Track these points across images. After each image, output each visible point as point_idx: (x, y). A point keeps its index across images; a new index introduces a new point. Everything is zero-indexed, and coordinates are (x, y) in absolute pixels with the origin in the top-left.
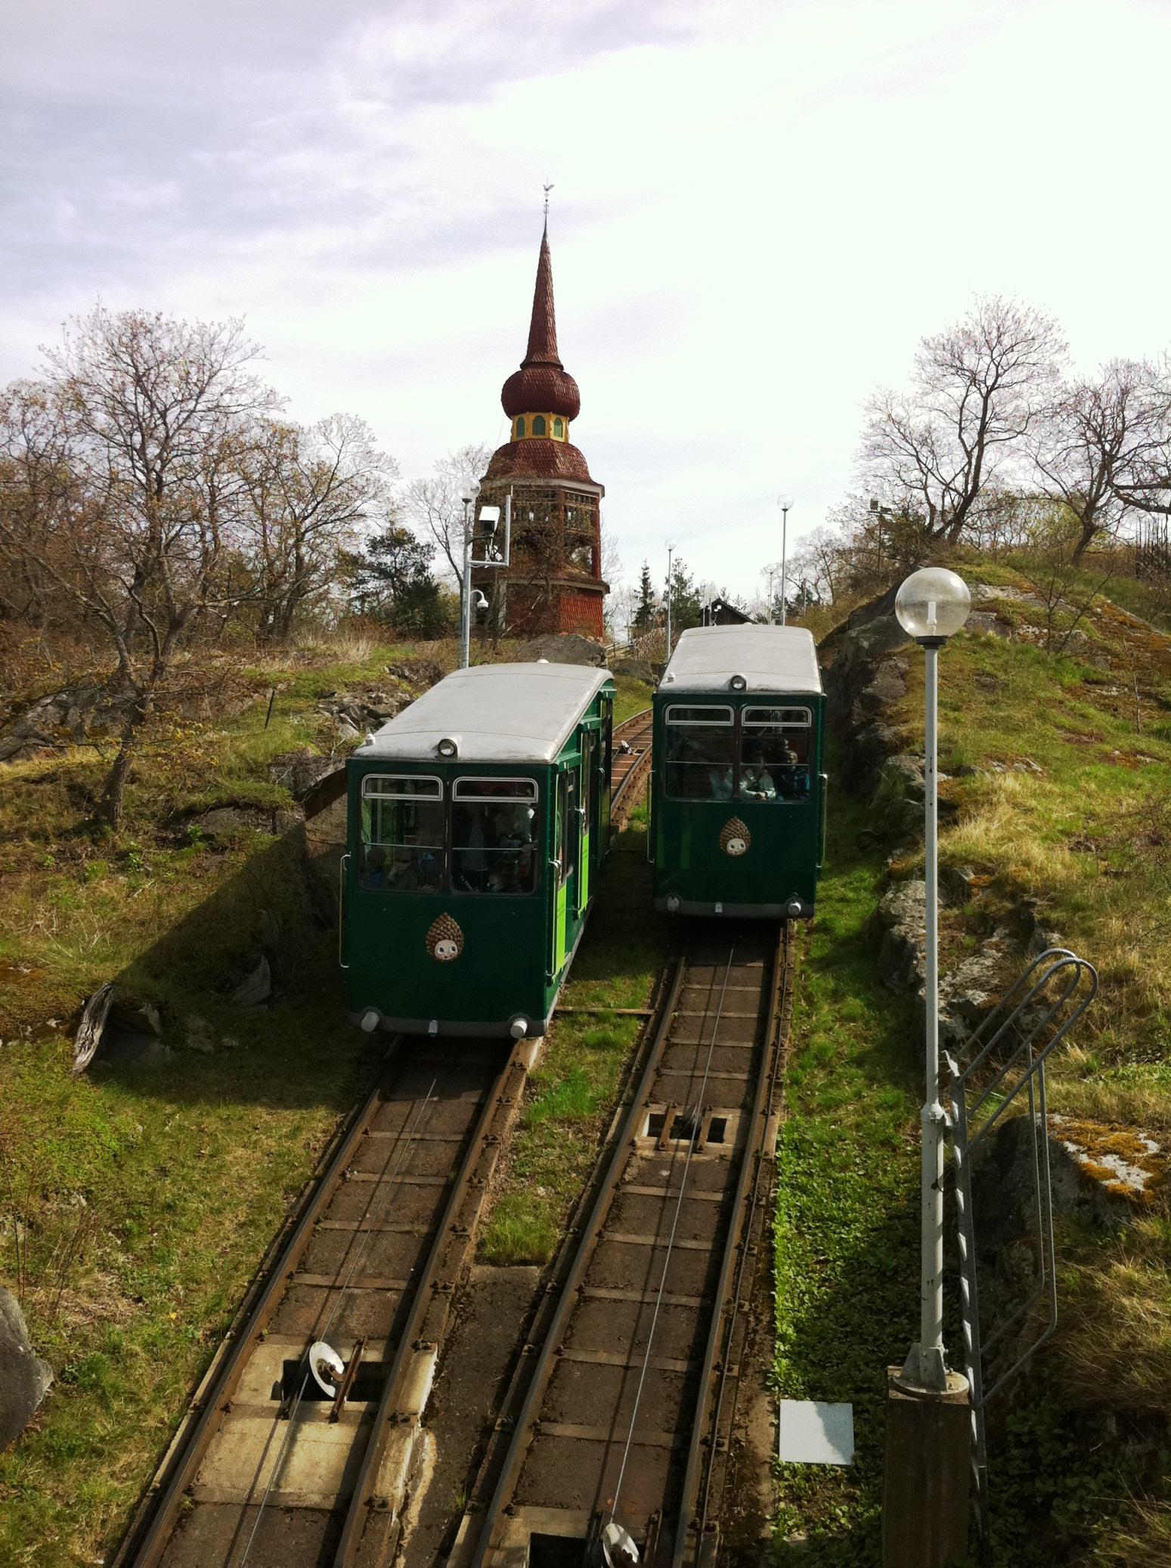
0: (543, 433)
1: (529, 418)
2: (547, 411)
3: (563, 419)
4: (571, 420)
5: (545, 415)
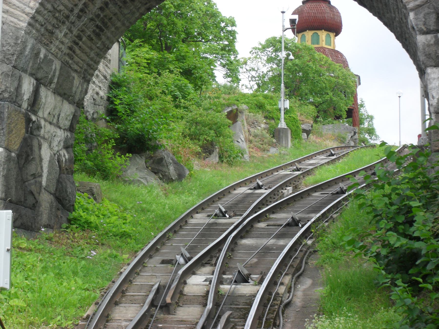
0: (318, 43)
1: (309, 34)
2: (320, 29)
3: (332, 35)
4: (336, 35)
5: (319, 32)
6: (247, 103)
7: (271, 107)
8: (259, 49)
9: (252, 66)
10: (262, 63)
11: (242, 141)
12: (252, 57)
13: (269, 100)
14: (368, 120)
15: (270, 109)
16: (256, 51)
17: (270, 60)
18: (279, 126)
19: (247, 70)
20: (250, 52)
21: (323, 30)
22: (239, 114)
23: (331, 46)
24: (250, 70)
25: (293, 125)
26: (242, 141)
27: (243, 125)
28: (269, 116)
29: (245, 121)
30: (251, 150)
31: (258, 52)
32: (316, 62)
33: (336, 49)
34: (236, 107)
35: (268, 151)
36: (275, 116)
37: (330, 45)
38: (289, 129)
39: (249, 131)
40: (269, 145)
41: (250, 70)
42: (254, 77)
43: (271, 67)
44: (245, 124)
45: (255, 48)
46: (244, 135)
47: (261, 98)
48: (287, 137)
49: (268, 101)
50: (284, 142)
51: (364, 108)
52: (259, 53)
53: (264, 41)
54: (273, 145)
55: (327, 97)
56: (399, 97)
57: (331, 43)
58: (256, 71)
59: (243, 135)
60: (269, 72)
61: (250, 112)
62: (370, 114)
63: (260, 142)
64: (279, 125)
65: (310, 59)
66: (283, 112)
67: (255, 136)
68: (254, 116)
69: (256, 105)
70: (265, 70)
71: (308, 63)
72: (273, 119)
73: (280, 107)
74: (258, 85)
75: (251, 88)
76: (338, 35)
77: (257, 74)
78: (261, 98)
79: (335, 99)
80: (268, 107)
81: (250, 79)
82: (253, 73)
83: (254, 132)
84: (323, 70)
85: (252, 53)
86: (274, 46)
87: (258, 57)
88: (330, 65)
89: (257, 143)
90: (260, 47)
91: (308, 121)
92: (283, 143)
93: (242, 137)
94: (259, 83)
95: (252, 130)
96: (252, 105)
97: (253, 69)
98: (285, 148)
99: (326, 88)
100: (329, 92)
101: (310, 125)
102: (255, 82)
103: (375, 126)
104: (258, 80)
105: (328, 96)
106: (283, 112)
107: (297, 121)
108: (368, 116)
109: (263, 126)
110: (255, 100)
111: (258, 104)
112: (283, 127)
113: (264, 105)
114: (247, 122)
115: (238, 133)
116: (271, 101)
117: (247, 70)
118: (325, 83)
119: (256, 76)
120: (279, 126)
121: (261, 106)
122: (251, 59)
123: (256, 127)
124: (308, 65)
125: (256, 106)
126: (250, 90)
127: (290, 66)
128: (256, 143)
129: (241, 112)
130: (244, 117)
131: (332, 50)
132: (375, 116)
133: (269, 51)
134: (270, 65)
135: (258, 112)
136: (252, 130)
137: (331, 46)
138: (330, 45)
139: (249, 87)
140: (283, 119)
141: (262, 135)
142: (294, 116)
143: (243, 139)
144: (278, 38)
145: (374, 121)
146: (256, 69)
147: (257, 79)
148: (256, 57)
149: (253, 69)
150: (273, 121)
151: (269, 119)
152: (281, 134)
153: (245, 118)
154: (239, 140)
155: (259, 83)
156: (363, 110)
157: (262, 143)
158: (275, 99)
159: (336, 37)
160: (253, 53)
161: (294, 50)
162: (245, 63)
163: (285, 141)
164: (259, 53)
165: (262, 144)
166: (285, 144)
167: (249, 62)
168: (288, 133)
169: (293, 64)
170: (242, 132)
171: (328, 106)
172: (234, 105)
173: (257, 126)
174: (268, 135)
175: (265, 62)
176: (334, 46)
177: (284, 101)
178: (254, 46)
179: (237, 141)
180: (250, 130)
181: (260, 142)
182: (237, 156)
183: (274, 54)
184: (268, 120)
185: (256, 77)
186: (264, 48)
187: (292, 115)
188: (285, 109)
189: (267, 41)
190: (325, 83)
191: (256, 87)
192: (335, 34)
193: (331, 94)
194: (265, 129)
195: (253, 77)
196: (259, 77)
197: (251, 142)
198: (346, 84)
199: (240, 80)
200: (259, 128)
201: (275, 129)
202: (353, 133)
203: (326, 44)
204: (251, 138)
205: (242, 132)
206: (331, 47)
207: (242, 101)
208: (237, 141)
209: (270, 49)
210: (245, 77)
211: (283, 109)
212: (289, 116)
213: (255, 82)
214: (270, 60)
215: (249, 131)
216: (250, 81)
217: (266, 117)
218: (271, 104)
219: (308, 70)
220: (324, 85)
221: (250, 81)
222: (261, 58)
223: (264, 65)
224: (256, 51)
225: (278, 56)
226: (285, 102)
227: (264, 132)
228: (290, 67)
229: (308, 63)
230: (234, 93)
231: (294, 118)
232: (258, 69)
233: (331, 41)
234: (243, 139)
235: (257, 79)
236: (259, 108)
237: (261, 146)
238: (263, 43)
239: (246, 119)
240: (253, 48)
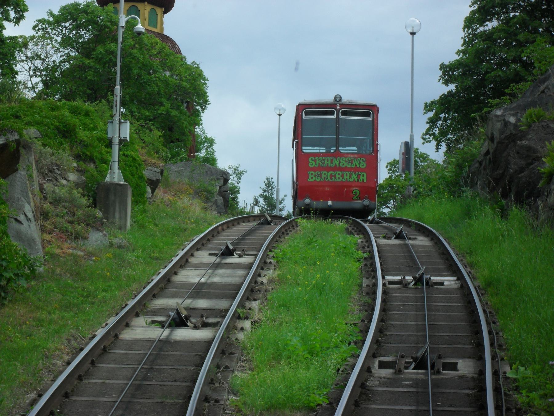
3: (159, 11)
4: (166, 12)
6: (38, 123)
7: (87, 133)
8: (49, 23)
9: (38, 49)
10: (53, 47)
11: (28, 220)
12: (37, 35)
13: (82, 117)
14: (205, 145)
15: (85, 139)
16: (44, 26)
17: (66, 42)
18: (108, 179)
19: (27, 57)
20: (34, 28)
21: (146, 3)
22: (22, 151)
23: (156, 28)
24: (33, 58)
25: (133, 175)
26: (28, 220)
27: (30, 177)
28: (84, 153)
29: (34, 167)
30: (48, 237)
31: (46, 28)
32: (143, 49)
33: (165, 33)
34: (17, 137)
35: (86, 238)
36: (96, 154)
37: (156, 26)
38: (129, 186)
39: (42, 189)
40: (88, 225)
41: (33, 58)
42: (39, 69)
43: (68, 55)
44: (35, 174)
45: (42, 21)
46: (32, 204)
47: (66, 113)
48: (124, 204)
49: (80, 120)
50: (117, 215)
51: (201, 127)
52: (49, 30)
53: (58, 9)
54: (98, 225)
55: (162, 110)
56: (280, 115)
57: (157, 23)
58: (43, 60)
59: (29, 204)
60: (64, 62)
61: (44, 145)
62: (209, 136)
63: (66, 218)
64: (108, 176)
65: (134, 46)
66: (116, 148)
67: (56, 202)
68: (53, 154)
69: (57, 128)
70: (57, 58)
71: (131, 50)
72: (91, 159)
73: (110, 136)
74: (45, 83)
75: (33, 88)
76: (168, 11)
77: (45, 65)
78: (66, 113)
79: (174, 113)
80: (83, 134)
81: (31, 73)
82: (38, 63)
83: (54, 192)
84: (156, 62)
85: (37, 29)
86: (75, 20)
87: (47, 36)
88: (167, 55)
89: (61, 220)
90: (51, 19)
91: (153, 161)
92: (114, 217)
93: (28, 209)
94: (46, 80)
95: (48, 186)
96: (49, 128)
97: (38, 57)
98: (120, 228)
99: (159, 93)
100: (164, 100)
101: (159, 170)
102: (40, 79)
103: (217, 155)
104: (45, 75)
105: (162, 108)
106: (116, 148)
107: (140, 165)
108: (206, 138)
109: (72, 177)
110: (55, 117)
111: (61, 128)
112: (116, 181)
113: (74, 130)
114: (37, 166)
115: (19, 199)
116: (87, 121)
117: (27, 57)
118: (158, 86)
119: (42, 68)
120: (108, 179)
121: (68, 131)
122: (35, 40)
123: (56, 179)
124: (131, 54)
125: (56, 132)
126: (31, 92)
127: (101, 53)
128: (58, 219)
129: (27, 147)
130: (33, 159)
131: (159, 34)
132: (217, 140)
133: (66, 28)
134: (66, 51)
135: (62, 144)
136: (48, 186)
137: (156, 28)
138: (156, 26)
139: (30, 85)
140: (117, 164)
141: (72, 201)
142: (134, 155)
143: (30, 215)
144: (82, 6)
145: (215, 147)
146: (43, 56)
147: (43, 73)
148: (43, 37)
149: (38, 57)
150: (92, 165)
151: (85, 161)
152: (112, 197)
153: (34, 161)
154: (22, 218)
155: (46, 80)
156: (198, 130)
157: (71, 219)
158: (94, 116)
159: (165, 15)
160: (39, 30)
161: (108, 28)
162: (25, 45)
163: (120, 212)
164: (49, 30)
165: (72, 223)
166: (120, 218)
167: (30, 45)
168: (126, 196)
169: (106, 51)
170: (27, 197)
171: (163, 125)
172: (12, 131)
173: (58, 177)
174: (84, 201)
175: (57, 46)
176: (162, 29)
177: (120, 123)
178: (39, 18)
179: (16, 220)
180: (45, 186)
181: (66, 218)
182: (17, 275)
183: (74, 32)
184: (82, 163)
185: (42, 71)
186: (58, 21)
187: (129, 152)
188: (122, 141)
189: (64, 9)
190: (158, 86)
191: (41, 86)
192: (163, 9)
193: (168, 105)
194: (77, 185)
195: (36, 69)
196: (46, 69)
197: (45, 215)
198: (195, 89)
199: (462, 38)
200: (64, 182)
201: (98, 184)
202: (222, 181)
203: (149, 25)
204: (46, 206)
205: (27, 197)
206: (157, 30)
207: (27, 119)
208: (16, 220)
209: (67, 24)
210: (23, 70)
211: (116, 140)
212: (124, 155)
213: (40, 79)
214: (66, 42)
215: (42, 189)
216: (31, 77)
217: (78, 157)
218: (86, 127)
219: (131, 62)
220: (156, 89)
221: (31, 77)
222: (51, 39)
223: (57, 50)
224: (44, 26)
225: (81, 36)
226: (123, 126)
227: (76, 193)
228: (100, 56)
229: (131, 50)
230: (9, 100)
231: (134, 159)
232: (46, 57)
233: (157, 20)
234: (30, 215)
235: (43, 73)
236: (64, 136)
237: (70, 227)
238: (56, 12)
239: (37, 162)
240: (40, 21)
